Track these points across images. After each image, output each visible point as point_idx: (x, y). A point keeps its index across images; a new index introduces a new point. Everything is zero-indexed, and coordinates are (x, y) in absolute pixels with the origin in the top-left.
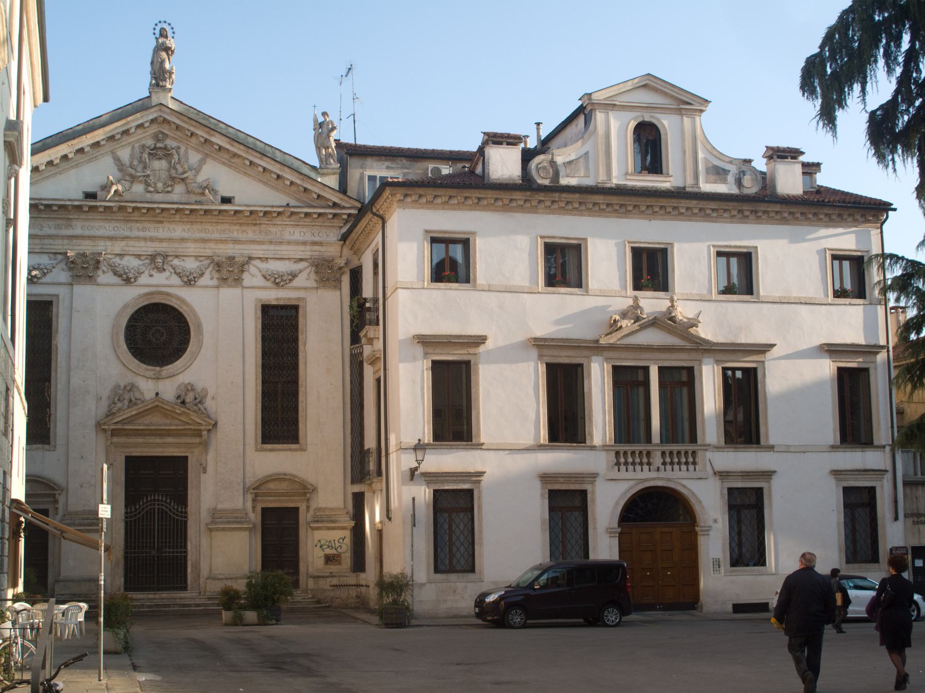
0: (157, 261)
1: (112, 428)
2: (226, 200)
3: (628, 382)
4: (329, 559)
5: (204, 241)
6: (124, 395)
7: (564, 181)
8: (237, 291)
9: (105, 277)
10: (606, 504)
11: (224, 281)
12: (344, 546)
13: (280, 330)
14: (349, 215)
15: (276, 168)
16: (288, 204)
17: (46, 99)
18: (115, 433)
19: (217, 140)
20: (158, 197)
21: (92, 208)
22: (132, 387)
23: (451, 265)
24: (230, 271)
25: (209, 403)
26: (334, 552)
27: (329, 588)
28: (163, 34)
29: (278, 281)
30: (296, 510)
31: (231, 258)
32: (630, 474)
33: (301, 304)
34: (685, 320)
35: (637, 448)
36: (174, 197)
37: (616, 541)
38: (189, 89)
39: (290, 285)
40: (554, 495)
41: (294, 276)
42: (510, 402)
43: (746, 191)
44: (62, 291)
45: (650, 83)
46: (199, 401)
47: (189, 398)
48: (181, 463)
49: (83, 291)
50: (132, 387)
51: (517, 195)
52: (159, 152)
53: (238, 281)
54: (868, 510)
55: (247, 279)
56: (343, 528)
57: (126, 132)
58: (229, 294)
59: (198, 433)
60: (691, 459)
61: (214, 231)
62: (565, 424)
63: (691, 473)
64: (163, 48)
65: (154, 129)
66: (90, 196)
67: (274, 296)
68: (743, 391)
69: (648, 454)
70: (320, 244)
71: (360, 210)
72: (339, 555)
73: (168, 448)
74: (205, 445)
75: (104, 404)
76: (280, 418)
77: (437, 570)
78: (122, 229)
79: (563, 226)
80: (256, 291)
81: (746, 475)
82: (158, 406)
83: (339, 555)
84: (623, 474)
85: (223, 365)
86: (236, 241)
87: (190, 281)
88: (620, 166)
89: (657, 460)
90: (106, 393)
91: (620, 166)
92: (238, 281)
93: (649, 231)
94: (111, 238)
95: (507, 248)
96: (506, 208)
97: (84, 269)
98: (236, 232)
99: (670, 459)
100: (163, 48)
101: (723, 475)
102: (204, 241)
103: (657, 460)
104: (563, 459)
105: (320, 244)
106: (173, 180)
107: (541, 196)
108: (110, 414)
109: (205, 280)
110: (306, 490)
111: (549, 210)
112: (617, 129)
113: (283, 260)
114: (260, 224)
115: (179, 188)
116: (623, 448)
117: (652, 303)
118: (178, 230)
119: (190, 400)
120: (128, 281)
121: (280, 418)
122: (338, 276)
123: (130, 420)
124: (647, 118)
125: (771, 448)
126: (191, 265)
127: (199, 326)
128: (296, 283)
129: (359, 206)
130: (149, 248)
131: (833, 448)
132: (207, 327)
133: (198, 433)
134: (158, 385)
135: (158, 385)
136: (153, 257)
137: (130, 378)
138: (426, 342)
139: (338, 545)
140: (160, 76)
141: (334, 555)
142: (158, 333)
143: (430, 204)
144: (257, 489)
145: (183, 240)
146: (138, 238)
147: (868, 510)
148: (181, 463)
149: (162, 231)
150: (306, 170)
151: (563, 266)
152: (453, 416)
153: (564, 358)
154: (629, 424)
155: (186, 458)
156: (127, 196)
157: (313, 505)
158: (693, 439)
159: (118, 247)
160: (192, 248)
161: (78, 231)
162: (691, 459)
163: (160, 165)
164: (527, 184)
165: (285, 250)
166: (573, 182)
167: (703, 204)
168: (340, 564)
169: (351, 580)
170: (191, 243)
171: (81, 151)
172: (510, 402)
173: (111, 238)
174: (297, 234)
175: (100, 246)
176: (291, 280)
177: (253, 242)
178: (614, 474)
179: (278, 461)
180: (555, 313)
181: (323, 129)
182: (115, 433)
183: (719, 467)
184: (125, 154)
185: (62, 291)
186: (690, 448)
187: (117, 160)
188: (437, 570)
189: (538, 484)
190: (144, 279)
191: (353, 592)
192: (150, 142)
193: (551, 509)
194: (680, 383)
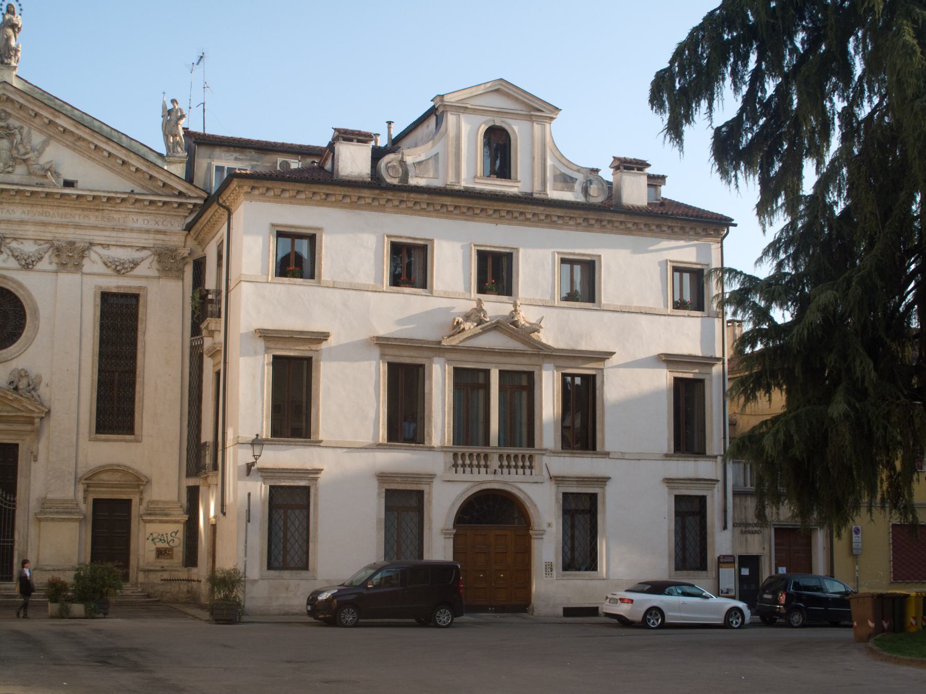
2: (69, 184)
3: (468, 384)
5: (44, 224)
7: (413, 181)
8: (77, 277)
10: (443, 504)
11: (63, 266)
13: (119, 318)
14: (195, 205)
16: (132, 191)
19: (62, 122)
24: (70, 257)
25: (43, 390)
26: (165, 545)
27: (160, 582)
29: (120, 268)
30: (129, 502)
31: (72, 243)
32: (467, 477)
33: (142, 293)
36: (15, 178)
39: (132, 273)
40: (390, 494)
41: (135, 264)
42: (351, 400)
45: (502, 88)
46: (33, 387)
47: (22, 385)
51: (366, 193)
53: (78, 267)
55: (87, 266)
58: (67, 279)
59: (30, 421)
60: (528, 464)
61: (55, 215)
62: (405, 417)
63: (528, 477)
67: (114, 283)
68: (582, 397)
69: (486, 456)
71: (206, 201)
72: (171, 549)
74: (37, 433)
76: (116, 409)
79: (410, 226)
81: (582, 480)
83: (171, 549)
84: (460, 476)
86: (77, 226)
87: (28, 264)
88: (469, 170)
89: (494, 463)
91: (469, 170)
92: (78, 267)
93: (496, 235)
95: (353, 245)
96: (354, 206)
99: (507, 463)
101: (558, 480)
102: (44, 224)
103: (494, 463)
104: (402, 459)
107: (389, 195)
109: (44, 264)
110: (139, 482)
111: (397, 209)
112: (468, 133)
113: (125, 249)
114: (103, 210)
115: (20, 169)
116: (461, 449)
117: (495, 307)
121: (116, 409)
122: (181, 266)
124: (498, 123)
125: (606, 454)
126: (29, 248)
127: (36, 311)
128: (137, 271)
131: (667, 456)
132: (44, 313)
133: (30, 421)
141: (166, 549)
144: (89, 480)
145: (22, 222)
150: (152, 157)
151: (408, 265)
152: (292, 410)
153: (406, 358)
155: (17, 445)
157: (147, 498)
158: (531, 443)
160: (31, 231)
162: (528, 464)
165: (127, 237)
168: (172, 558)
169: (183, 574)
172: (351, 400)
174: (141, 222)
176: (132, 268)
177: (95, 227)
178: (452, 475)
180: (398, 313)
181: (171, 117)
183: (554, 472)
186: (527, 452)
188: (270, 567)
189: (375, 483)
191: (184, 587)
193: (388, 509)
194: (520, 387)
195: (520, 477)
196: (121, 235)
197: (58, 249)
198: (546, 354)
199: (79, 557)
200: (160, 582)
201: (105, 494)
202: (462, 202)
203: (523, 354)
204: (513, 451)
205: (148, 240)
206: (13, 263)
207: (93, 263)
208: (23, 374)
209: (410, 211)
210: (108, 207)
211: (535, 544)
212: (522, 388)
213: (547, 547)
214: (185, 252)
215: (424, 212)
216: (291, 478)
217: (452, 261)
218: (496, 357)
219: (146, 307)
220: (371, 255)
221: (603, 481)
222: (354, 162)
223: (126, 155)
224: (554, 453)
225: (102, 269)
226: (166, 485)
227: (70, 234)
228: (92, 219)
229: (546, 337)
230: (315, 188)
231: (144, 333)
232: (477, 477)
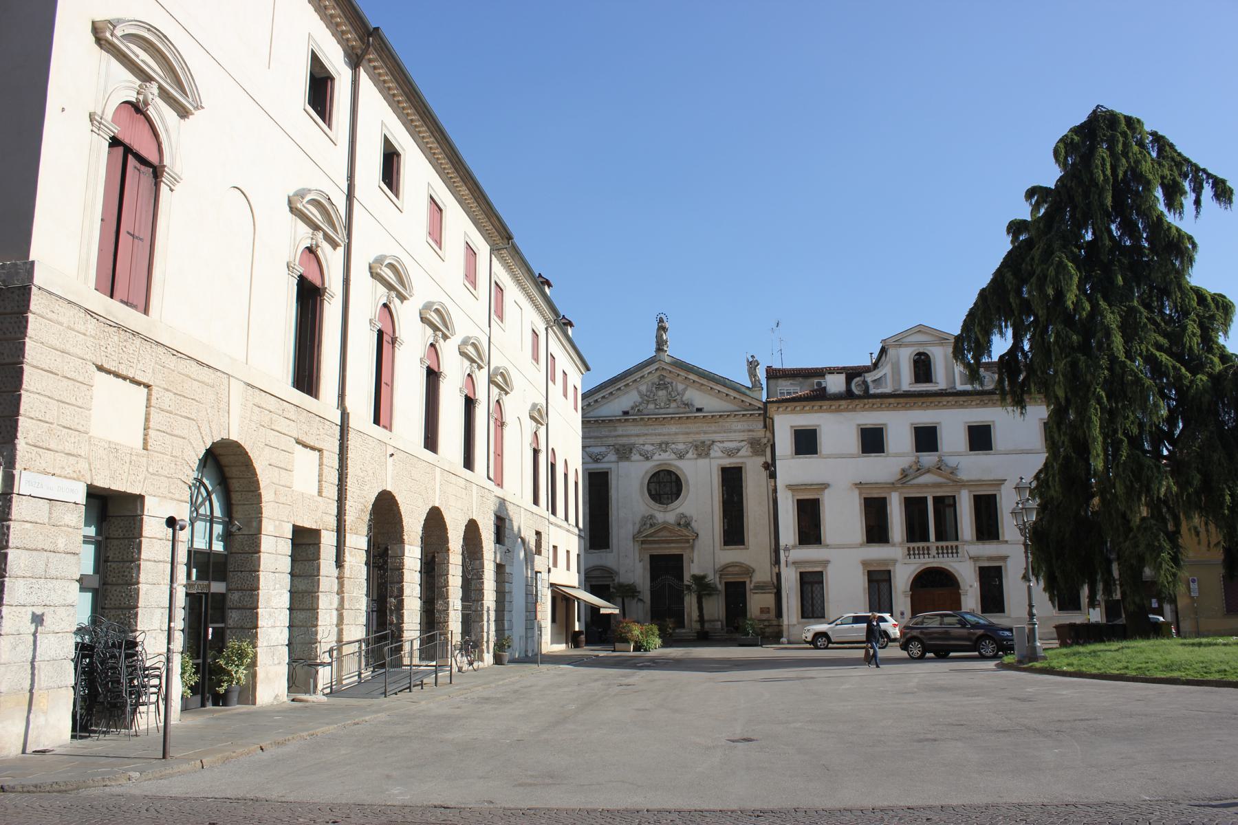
0: (663, 446)
1: (642, 539)
2: (699, 410)
3: (914, 507)
4: (763, 610)
5: (688, 434)
6: (648, 521)
7: (872, 391)
8: (707, 460)
9: (635, 456)
10: (903, 578)
11: (699, 456)
13: (732, 479)
15: (725, 390)
17: (588, 369)
18: (643, 542)
19: (692, 377)
20: (662, 411)
21: (626, 420)
22: (652, 517)
23: (806, 442)
24: (703, 450)
25: (693, 524)
28: (661, 320)
29: (730, 453)
30: (744, 583)
31: (703, 442)
32: (917, 560)
34: (516, 529)
35: (949, 544)
36: (670, 411)
37: (909, 600)
38: (676, 349)
40: (870, 573)
42: (843, 519)
43: (986, 388)
44: (613, 466)
45: (921, 329)
46: (687, 525)
47: (682, 522)
48: (680, 558)
49: (624, 465)
50: (652, 517)
51: (843, 403)
52: (662, 385)
53: (707, 455)
55: (712, 454)
57: (642, 377)
58: (703, 462)
59: (688, 541)
60: (955, 551)
61: (693, 427)
62: (876, 531)
63: (955, 559)
64: (662, 328)
65: (658, 373)
66: (626, 413)
67: (728, 462)
68: (986, 508)
69: (928, 548)
73: (673, 550)
74: (692, 547)
75: (637, 527)
76: (734, 533)
77: (803, 617)
78: (644, 430)
79: (871, 418)
80: (718, 460)
81: (990, 559)
82: (665, 527)
84: (912, 560)
85: (701, 501)
86: (705, 433)
87: (681, 456)
88: (907, 382)
89: (933, 552)
90: (638, 519)
91: (907, 382)
92: (707, 455)
93: (925, 416)
94: (637, 436)
95: (838, 430)
96: (838, 410)
97: (624, 453)
98: (705, 427)
99: (941, 551)
100: (662, 328)
101: (975, 559)
102: (688, 434)
103: (933, 552)
104: (877, 552)
106: (670, 400)
107: (857, 402)
108: (639, 532)
109: (690, 455)
110: (749, 571)
111: (863, 409)
112: (905, 357)
113: (730, 445)
115: (673, 405)
116: (912, 545)
117: (928, 459)
118: (673, 428)
119: (685, 523)
120: (647, 459)
121: (734, 533)
123: (651, 535)
124: (921, 350)
125: (827, 546)
126: (681, 447)
127: (687, 481)
128: (740, 454)
130: (658, 440)
131: (861, 545)
132: (691, 482)
133: (688, 541)
134: (667, 515)
135: (667, 515)
136: (660, 445)
137: (651, 512)
138: (790, 487)
140: (660, 345)
142: (666, 486)
143: (793, 411)
144: (723, 571)
145: (676, 434)
146: (651, 435)
148: (680, 558)
149: (665, 430)
150: (744, 389)
151: (872, 441)
152: (810, 530)
153: (875, 494)
154: (916, 531)
155: (681, 556)
156: (645, 411)
157: (754, 580)
158: (957, 539)
159: (641, 440)
160: (681, 438)
161: (620, 433)
162: (955, 551)
163: (662, 393)
164: (849, 395)
165: (733, 436)
166: (879, 391)
167: (956, 398)
170: (679, 435)
171: (596, 401)
172: (843, 519)
173: (637, 436)
174: (740, 426)
175: (633, 440)
177: (715, 432)
178: (907, 561)
179: (732, 555)
180: (880, 469)
181: (752, 365)
182: (643, 542)
183: (972, 554)
184: (643, 388)
185: (613, 466)
186: (954, 543)
187: (639, 392)
188: (803, 617)
189: (861, 567)
190: (655, 457)
192: (656, 380)
193: (869, 581)
194: (945, 505)
195: (946, 559)
197: (696, 447)
198: (963, 484)
201: (731, 579)
202: (902, 400)
203: (946, 485)
204: (944, 544)
205: (745, 436)
206: (673, 456)
207: (716, 451)
208: (683, 516)
209: (872, 409)
211: (963, 598)
212: (950, 506)
213: (971, 600)
214: (765, 441)
215: (880, 409)
216: (480, 576)
217: (899, 435)
218: (928, 486)
220: (337, 457)
221: (826, 563)
222: (835, 384)
224: (971, 543)
225: (720, 454)
226: (763, 574)
227: (703, 437)
228: (713, 427)
229: (963, 476)
230: (813, 403)
232: (923, 561)
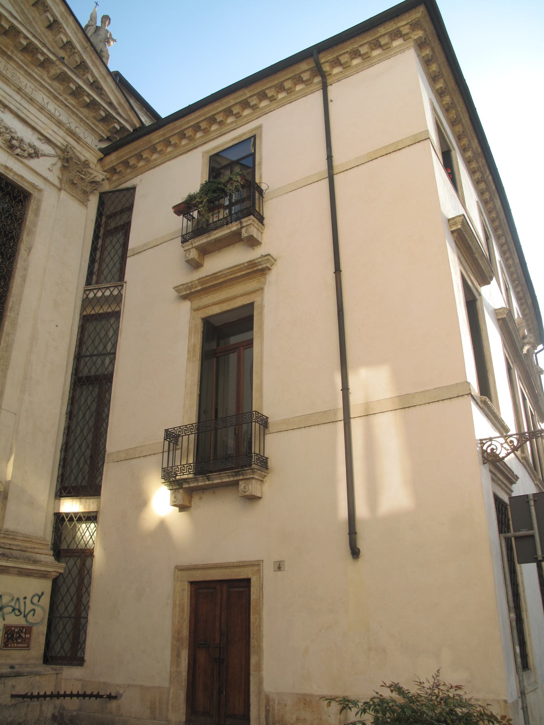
12: (39, 611)
14: (123, 128)
16: (63, 58)
26: (20, 621)
27: (8, 701)
33: (35, 194)
39: (25, 161)
41: (36, 154)
54: (64, 546)
56: (43, 575)
70: (78, 139)
71: (135, 130)
72: (28, 629)
83: (28, 629)
105: (78, 139)
114: (10, 58)
122: (88, 189)
128: (33, 163)
129: (138, 125)
139: (29, 606)
141: (21, 628)
147: (64, 546)
168: (28, 647)
169: (46, 681)
176: (30, 156)
191: (49, 708)
196: (26, 104)
199: (50, 555)
200: (8, 701)
205: (60, 137)
210: (19, 57)
219: (37, 213)
223: (62, 15)
231: (30, 249)
